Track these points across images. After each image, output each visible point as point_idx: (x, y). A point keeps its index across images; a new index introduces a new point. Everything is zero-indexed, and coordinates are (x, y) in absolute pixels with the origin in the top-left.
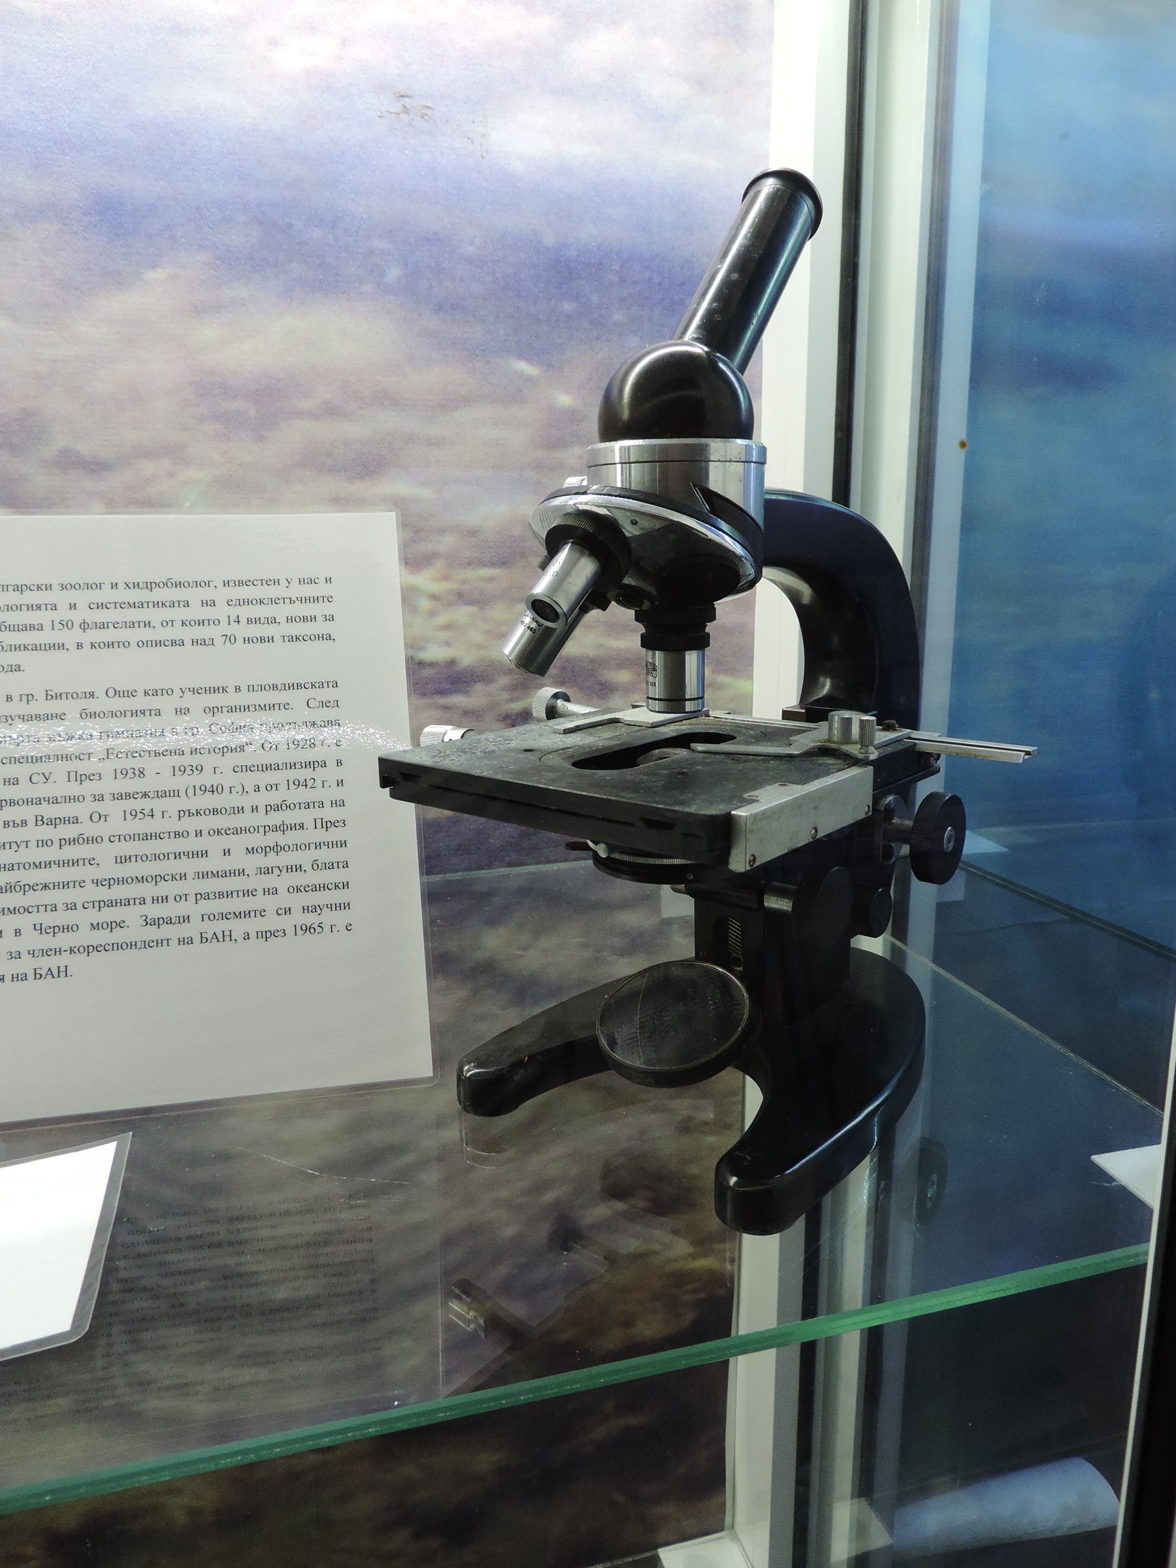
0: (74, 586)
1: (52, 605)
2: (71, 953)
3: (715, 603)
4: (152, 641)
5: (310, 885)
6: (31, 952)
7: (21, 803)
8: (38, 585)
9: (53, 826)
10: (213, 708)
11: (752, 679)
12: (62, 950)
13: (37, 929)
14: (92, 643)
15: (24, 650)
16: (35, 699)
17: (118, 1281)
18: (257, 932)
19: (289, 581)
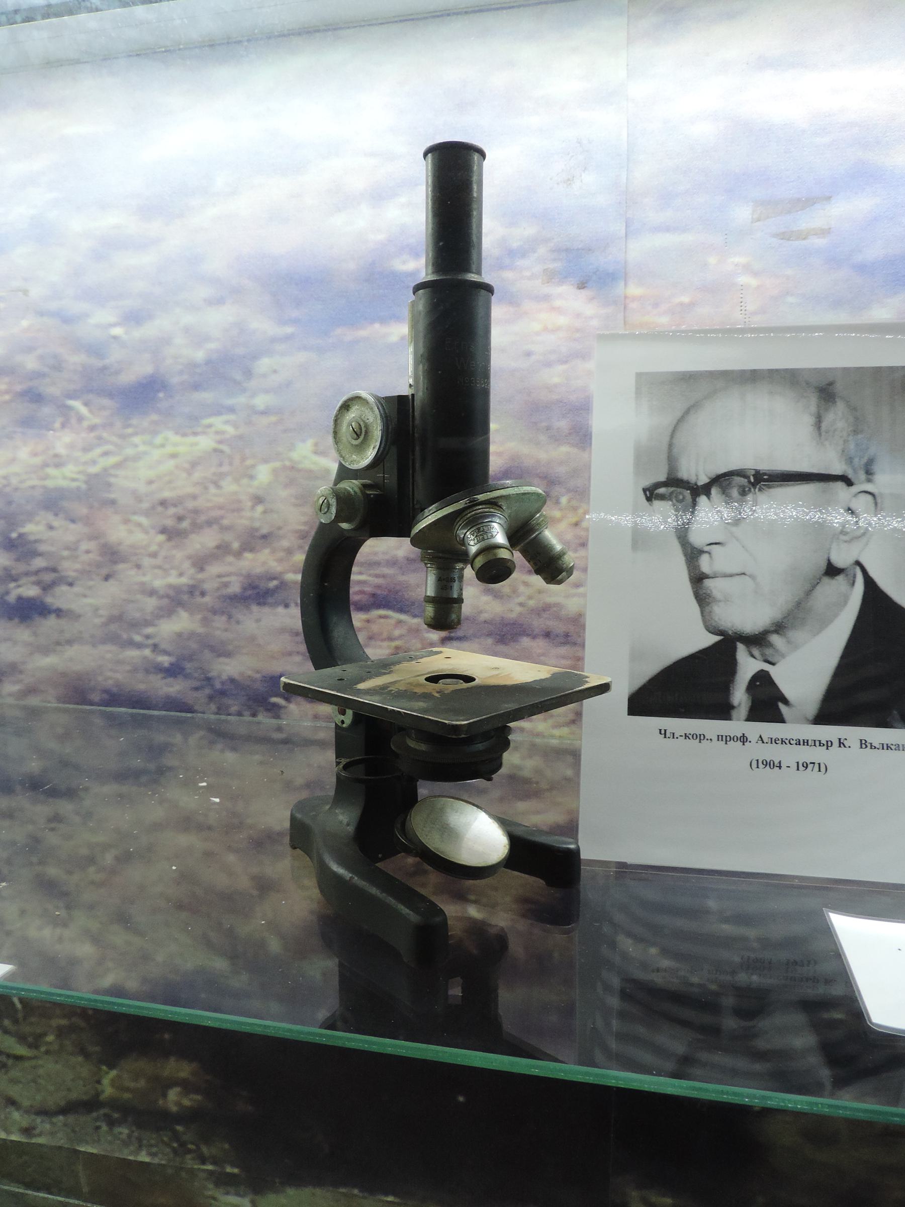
0: (737, 740)
1: (895, 745)
2: (686, 738)
3: (511, 725)
4: (722, 736)
5: (794, 739)
6: (663, 732)
7: (735, 740)
8: (782, 739)
9: (724, 742)
10: (700, 735)
11: (582, 727)
12: (684, 737)
13: (662, 733)
14: (840, 739)
15: (887, 749)
16: (706, 738)
17: (802, 601)
18: (718, 736)
19: (760, 739)
